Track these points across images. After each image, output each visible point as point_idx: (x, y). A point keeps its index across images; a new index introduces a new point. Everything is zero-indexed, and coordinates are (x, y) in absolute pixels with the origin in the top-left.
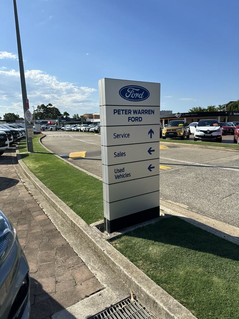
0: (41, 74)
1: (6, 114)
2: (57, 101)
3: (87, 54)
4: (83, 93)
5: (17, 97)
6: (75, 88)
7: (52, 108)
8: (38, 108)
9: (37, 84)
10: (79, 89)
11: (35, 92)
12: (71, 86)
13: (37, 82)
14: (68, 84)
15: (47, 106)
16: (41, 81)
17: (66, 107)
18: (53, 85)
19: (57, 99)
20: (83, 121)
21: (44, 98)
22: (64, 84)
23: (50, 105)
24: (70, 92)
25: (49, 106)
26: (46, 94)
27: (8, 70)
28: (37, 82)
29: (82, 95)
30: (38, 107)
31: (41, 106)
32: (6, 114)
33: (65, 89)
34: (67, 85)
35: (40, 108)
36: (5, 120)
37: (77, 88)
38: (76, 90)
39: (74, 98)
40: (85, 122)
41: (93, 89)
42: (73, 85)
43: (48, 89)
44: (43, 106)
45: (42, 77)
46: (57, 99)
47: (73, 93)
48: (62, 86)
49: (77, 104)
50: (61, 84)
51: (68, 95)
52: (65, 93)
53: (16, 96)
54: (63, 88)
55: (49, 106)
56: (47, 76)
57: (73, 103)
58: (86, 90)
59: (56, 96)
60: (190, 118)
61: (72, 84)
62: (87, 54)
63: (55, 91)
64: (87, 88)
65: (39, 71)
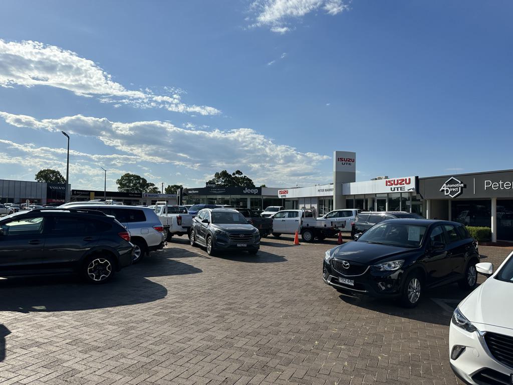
0: (253, 134)
1: (169, 186)
2: (268, 173)
3: (328, 105)
4: (310, 161)
5: (214, 167)
6: (298, 154)
7: (242, 178)
8: (215, 176)
9: (246, 148)
10: (304, 155)
11: (240, 159)
12: (292, 151)
13: (245, 146)
14: (289, 148)
15: (234, 174)
16: (252, 145)
17: (279, 182)
18: (267, 150)
19: (269, 170)
20: (251, 194)
21: (251, 168)
22: (283, 147)
23: (238, 172)
24: (289, 160)
25: (237, 175)
26: (254, 163)
27: (210, 130)
28: (245, 146)
29: (307, 165)
30: (217, 175)
31: (221, 173)
32: (169, 186)
33: (283, 156)
34: (287, 151)
35: (219, 178)
36: (123, 190)
37: (301, 155)
38: (299, 157)
39: (293, 169)
40: (258, 197)
41: (325, 157)
42: (295, 150)
43: (259, 156)
44: (225, 174)
45: (254, 138)
46: (269, 170)
47: (293, 161)
48: (280, 150)
49: (296, 178)
50: (279, 148)
51: (286, 165)
52: (282, 161)
53: (213, 166)
54: (280, 154)
55: (237, 175)
56: (261, 137)
57: (292, 176)
58: (314, 158)
59: (267, 165)
60: (389, 253)
61: (295, 148)
62: (328, 105)
63: (268, 159)
64: (318, 154)
65: (250, 130)
